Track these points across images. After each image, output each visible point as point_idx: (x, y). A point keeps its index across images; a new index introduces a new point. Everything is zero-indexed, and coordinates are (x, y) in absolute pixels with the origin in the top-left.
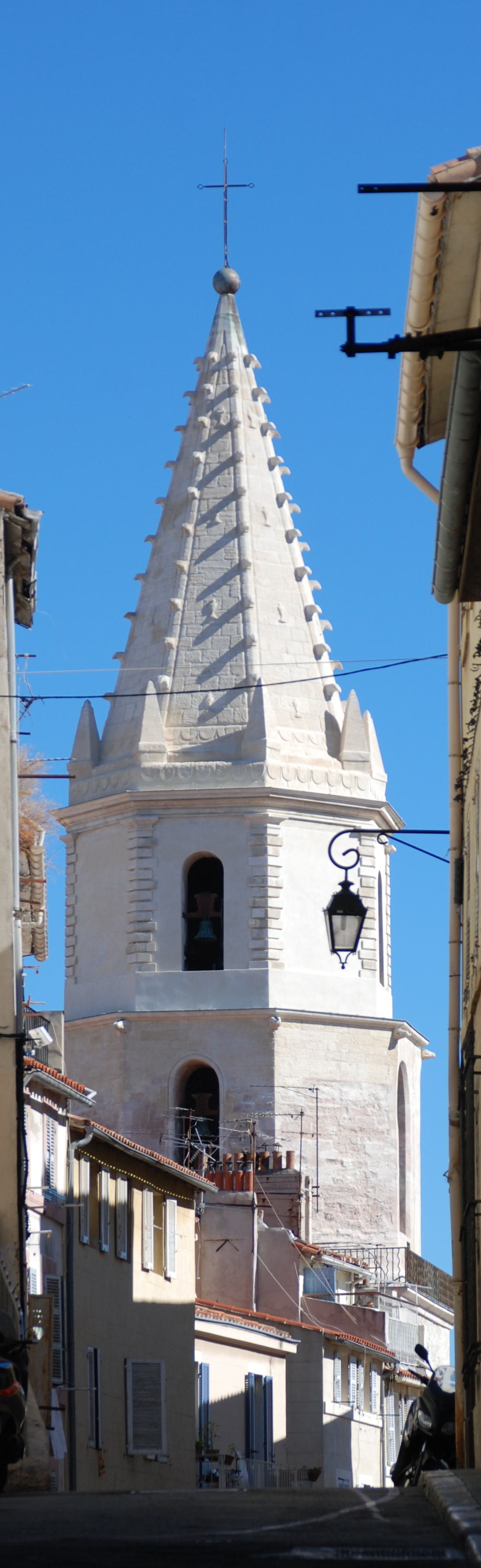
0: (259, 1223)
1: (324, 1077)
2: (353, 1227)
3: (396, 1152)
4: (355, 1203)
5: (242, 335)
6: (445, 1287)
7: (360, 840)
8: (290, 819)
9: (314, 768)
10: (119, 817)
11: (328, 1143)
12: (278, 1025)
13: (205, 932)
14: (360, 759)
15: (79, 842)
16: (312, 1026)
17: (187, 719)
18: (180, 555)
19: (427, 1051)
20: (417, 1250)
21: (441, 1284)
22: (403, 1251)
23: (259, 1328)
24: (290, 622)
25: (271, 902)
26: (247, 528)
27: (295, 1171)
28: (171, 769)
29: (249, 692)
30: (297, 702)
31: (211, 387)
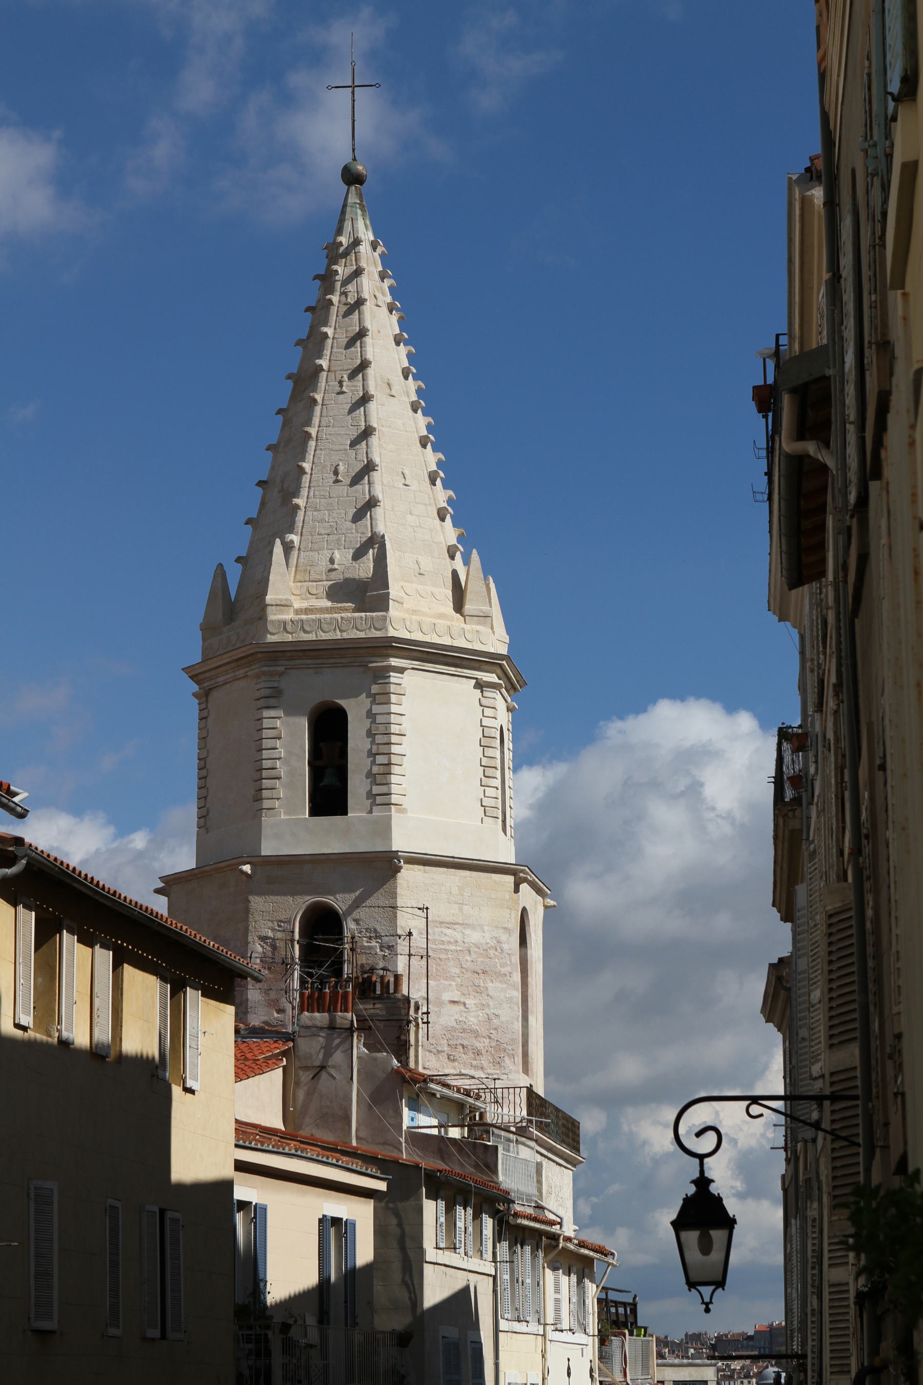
0: (359, 1048)
1: (447, 919)
2: (476, 1068)
3: (518, 995)
4: (478, 1044)
5: (368, 222)
6: (568, 1129)
7: (482, 692)
8: (413, 669)
9: (437, 621)
10: (246, 670)
11: (450, 985)
12: (401, 868)
13: (329, 779)
14: (482, 614)
15: (210, 698)
16: (434, 869)
17: (314, 576)
18: (309, 423)
19: (549, 900)
20: (540, 1090)
21: (563, 1125)
22: (524, 1091)
23: (328, 1158)
24: (414, 486)
25: (394, 749)
26: (372, 396)
27: (404, 996)
28: (297, 621)
29: (373, 548)
30: (420, 559)
31: (340, 269)
